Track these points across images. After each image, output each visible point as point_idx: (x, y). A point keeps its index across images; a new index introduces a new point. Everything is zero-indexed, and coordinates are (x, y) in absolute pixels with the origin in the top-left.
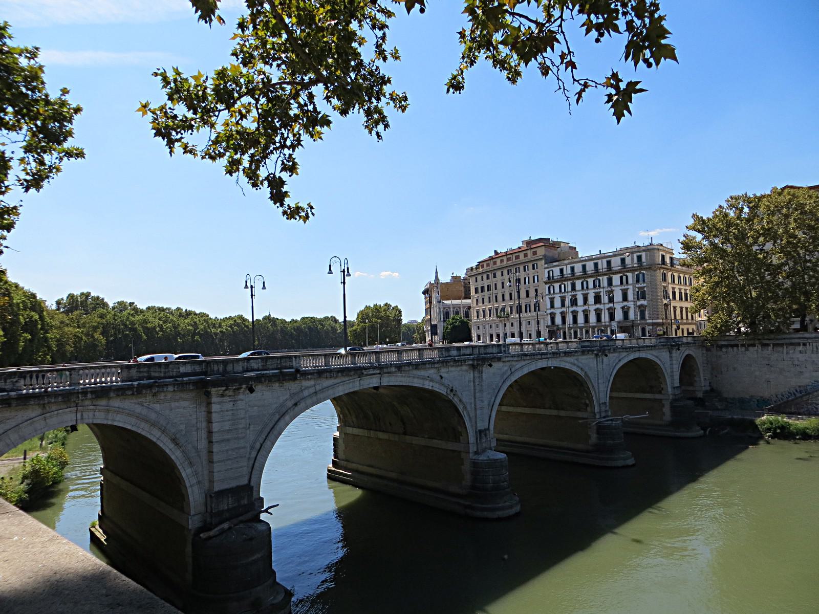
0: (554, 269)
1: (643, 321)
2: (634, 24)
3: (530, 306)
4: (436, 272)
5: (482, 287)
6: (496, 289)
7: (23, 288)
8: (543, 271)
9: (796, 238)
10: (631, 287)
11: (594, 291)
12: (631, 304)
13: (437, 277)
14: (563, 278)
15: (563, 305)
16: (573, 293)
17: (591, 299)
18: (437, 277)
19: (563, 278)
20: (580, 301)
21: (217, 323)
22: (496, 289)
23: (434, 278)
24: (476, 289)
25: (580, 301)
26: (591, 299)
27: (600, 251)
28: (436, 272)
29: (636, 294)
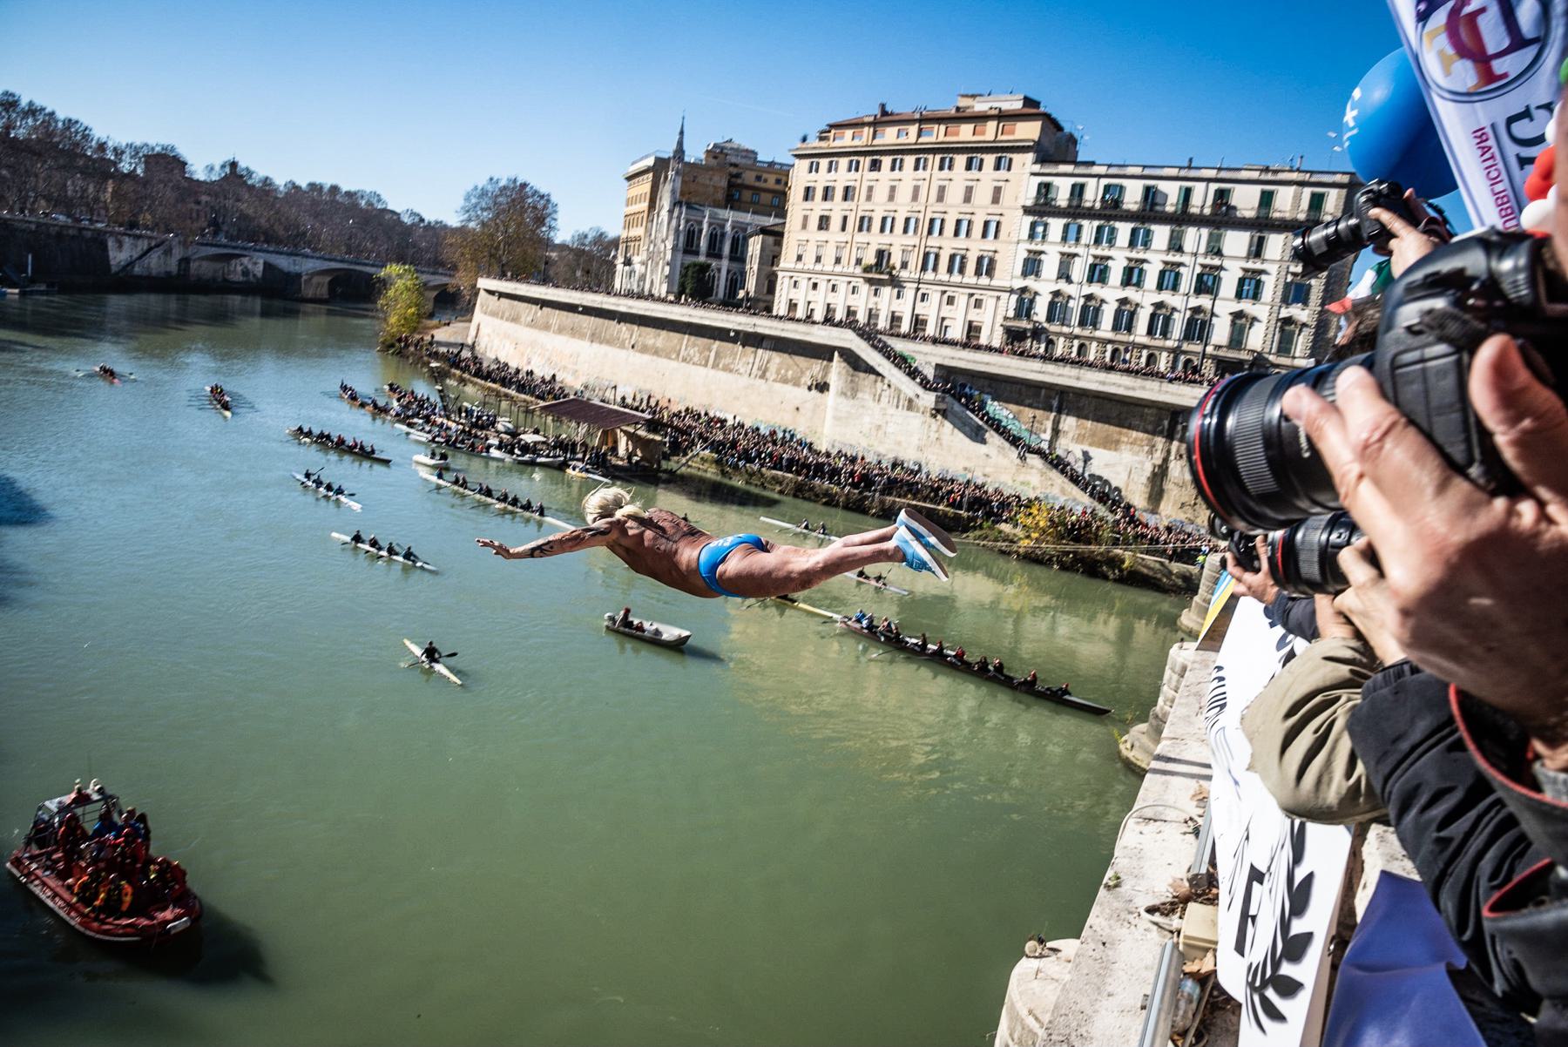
0: (1056, 181)
1: (1123, 337)
2: (43, 288)
3: (937, 256)
4: (682, 133)
5: (827, 189)
6: (869, 198)
7: (43, 109)
8: (1024, 177)
9: (106, 176)
10: (1273, 268)
11: (1093, 251)
12: (1260, 310)
13: (680, 143)
14: (1076, 211)
15: (1064, 275)
16: (1208, 261)
17: (1079, 270)
18: (680, 143)
19: (1076, 211)
20: (1050, 266)
21: (266, 189)
22: (869, 198)
23: (674, 146)
24: (808, 194)
25: (1050, 266)
26: (1079, 270)
27: (1191, 160)
28: (682, 133)
29: (1281, 287)
